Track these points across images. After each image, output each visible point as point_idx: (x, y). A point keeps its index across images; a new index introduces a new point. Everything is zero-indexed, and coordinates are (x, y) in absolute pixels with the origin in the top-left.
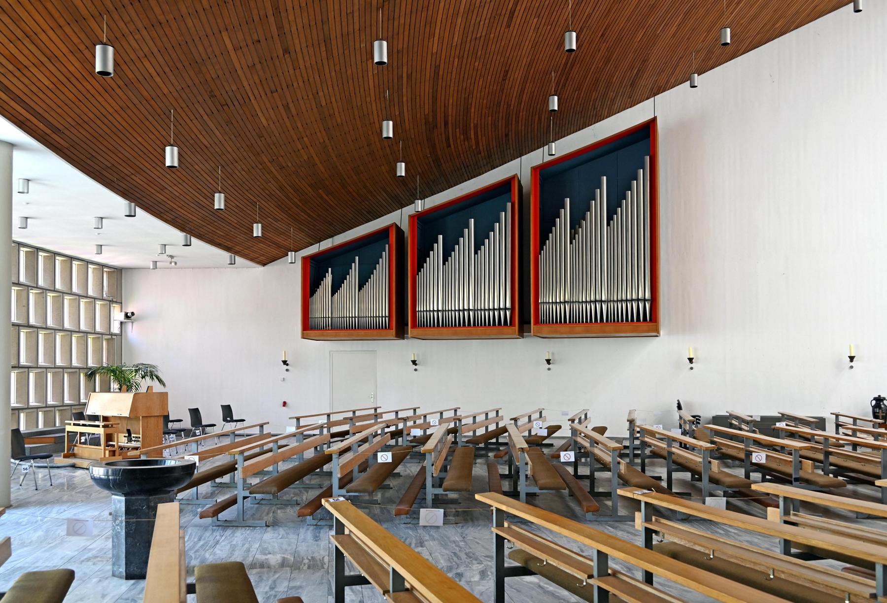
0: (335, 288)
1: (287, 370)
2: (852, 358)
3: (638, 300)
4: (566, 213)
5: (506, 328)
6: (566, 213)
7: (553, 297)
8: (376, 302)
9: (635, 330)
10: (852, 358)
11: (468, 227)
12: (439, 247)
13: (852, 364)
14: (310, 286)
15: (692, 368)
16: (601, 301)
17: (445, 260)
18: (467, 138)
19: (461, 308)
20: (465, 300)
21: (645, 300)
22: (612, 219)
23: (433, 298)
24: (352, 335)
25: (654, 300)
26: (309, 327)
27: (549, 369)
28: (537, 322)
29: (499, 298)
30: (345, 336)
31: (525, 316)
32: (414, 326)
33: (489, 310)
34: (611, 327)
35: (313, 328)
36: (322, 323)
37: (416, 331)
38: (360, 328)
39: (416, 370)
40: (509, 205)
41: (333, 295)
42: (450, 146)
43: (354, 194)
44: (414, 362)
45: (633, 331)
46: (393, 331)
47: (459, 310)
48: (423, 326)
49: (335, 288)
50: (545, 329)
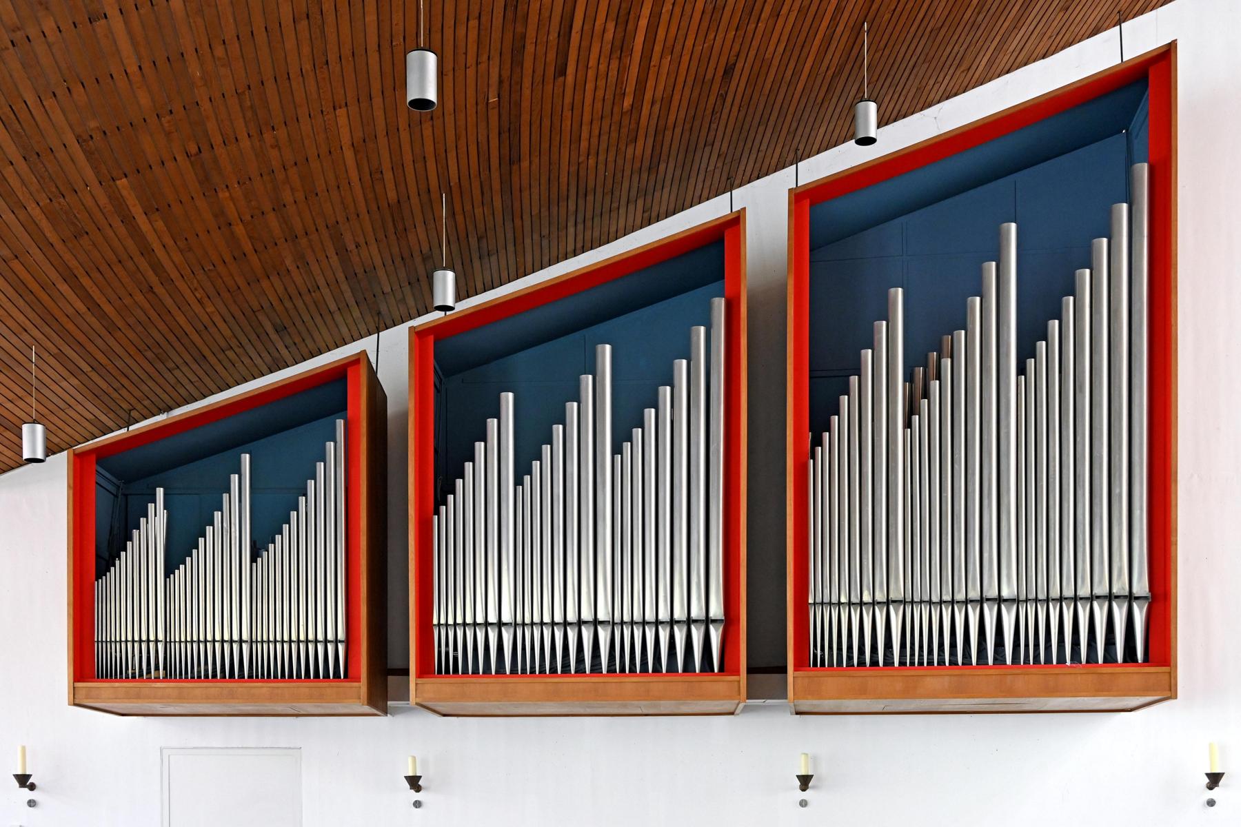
0: (178, 552)
1: (32, 803)
2: (1214, 779)
3: (1110, 597)
4: (892, 334)
5: (707, 678)
6: (892, 334)
7: (851, 588)
8: (308, 599)
9: (1101, 689)
10: (1214, 779)
11: (593, 369)
12: (503, 430)
13: (1214, 794)
14: (97, 549)
15: (1211, 803)
16: (1000, 600)
17: (522, 470)
18: (621, 47)
19: (572, 617)
20: (586, 595)
21: (1131, 598)
22: (1033, 355)
23: (482, 592)
24: (232, 696)
25: (1161, 599)
26: (91, 665)
27: (803, 803)
28: (801, 664)
29: (687, 591)
30: (208, 698)
31: (767, 645)
32: (425, 670)
33: (657, 623)
34: (1035, 676)
35: (110, 673)
36: (134, 657)
37: (434, 687)
38: (258, 673)
39: (417, 804)
40: (719, 304)
41: (169, 572)
42: (562, 72)
43: (239, 230)
44: (414, 782)
45: (1098, 691)
46: (363, 686)
47: (580, 623)
48: (450, 669)
49: (178, 552)
50: (830, 680)
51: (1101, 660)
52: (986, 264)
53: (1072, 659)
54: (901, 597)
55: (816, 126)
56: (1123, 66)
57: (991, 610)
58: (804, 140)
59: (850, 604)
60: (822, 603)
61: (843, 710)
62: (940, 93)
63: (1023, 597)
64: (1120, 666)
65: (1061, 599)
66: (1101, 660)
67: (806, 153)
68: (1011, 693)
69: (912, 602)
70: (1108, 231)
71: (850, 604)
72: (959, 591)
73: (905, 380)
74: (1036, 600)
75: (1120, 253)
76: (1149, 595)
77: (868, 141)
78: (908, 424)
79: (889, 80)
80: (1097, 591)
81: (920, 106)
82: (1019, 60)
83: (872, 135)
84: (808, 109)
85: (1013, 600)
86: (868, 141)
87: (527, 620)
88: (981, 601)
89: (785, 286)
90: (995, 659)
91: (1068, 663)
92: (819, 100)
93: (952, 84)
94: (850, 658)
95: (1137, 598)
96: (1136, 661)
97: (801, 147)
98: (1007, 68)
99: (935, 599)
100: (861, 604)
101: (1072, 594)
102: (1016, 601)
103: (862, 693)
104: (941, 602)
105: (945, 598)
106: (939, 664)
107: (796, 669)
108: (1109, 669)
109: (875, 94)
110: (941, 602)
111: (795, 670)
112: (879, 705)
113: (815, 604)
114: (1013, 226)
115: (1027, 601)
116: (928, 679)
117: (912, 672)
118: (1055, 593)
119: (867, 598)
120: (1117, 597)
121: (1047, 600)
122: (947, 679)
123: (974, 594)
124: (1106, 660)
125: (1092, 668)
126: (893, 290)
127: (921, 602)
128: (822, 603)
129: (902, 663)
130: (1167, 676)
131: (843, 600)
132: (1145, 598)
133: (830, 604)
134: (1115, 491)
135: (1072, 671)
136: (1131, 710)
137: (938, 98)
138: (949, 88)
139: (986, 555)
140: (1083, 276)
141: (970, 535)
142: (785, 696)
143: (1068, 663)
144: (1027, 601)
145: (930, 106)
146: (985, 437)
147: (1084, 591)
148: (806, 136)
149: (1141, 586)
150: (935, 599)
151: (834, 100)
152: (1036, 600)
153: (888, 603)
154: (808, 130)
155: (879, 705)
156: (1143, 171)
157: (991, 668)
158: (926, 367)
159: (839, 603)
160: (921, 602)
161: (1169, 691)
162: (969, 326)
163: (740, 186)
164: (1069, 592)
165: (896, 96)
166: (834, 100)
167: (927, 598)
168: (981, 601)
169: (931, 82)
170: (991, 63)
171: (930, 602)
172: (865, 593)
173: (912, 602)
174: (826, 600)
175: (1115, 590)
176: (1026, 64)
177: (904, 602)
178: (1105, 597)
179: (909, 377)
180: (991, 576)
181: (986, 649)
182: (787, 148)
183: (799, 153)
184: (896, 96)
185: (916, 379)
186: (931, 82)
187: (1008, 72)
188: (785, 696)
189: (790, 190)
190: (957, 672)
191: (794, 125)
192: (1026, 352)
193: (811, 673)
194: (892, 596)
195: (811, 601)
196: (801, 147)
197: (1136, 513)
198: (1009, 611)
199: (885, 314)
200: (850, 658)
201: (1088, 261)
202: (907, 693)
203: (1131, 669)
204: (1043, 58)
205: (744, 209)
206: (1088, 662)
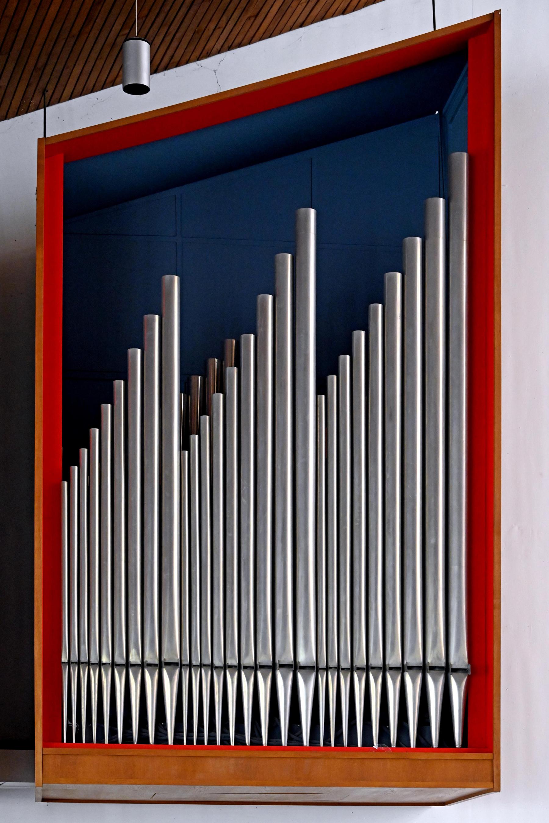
4: (166, 333)
6: (166, 333)
21: (447, 670)
28: (53, 737)
50: (90, 761)
51: (413, 744)
52: (280, 256)
53: (380, 742)
54: (177, 659)
55: (70, 64)
56: (434, 37)
57: (285, 679)
58: (54, 81)
59: (113, 664)
60: (79, 663)
61: (102, 798)
62: (221, 41)
63: (322, 664)
64: (435, 750)
65: (367, 669)
66: (413, 744)
67: (56, 96)
68: (309, 781)
69: (190, 666)
70: (422, 230)
71: (113, 664)
72: (247, 653)
73: (181, 391)
74: (338, 668)
75: (434, 259)
76: (469, 667)
77: (139, 89)
78: (185, 445)
79: (162, 16)
80: (409, 661)
81: (197, 53)
82: (262, 30)
83: (145, 82)
84: (61, 43)
85: (311, 668)
86: (139, 89)
87: (361, 661)
88: (273, 667)
89: (33, 259)
90: (290, 739)
91: (376, 746)
92: (75, 31)
93: (235, 32)
94: (338, 735)
95: (455, 671)
96: (453, 744)
97: (51, 88)
98: (301, 20)
99: (218, 662)
100: (128, 665)
101: (380, 663)
102: (314, 668)
103: (129, 776)
104: (225, 667)
105: (230, 662)
106: (222, 742)
107: (45, 745)
108: (423, 755)
109: (144, 32)
110: (225, 667)
111: (45, 745)
112: (148, 792)
113: (69, 663)
114: (312, 212)
115: (327, 668)
116: (210, 761)
117: (191, 753)
118: (361, 661)
119: (134, 658)
120: (432, 668)
121: (351, 669)
122: (232, 761)
123: (265, 659)
124: (419, 744)
125: (403, 753)
126: (167, 277)
127: (201, 666)
128: (79, 663)
129: (178, 740)
130: (488, 765)
131: (104, 660)
132: (464, 670)
133: (89, 663)
134: (430, 541)
135: (380, 755)
136: (444, 804)
137: (218, 46)
138: (232, 37)
139: (279, 611)
140: (265, 302)
141: (260, 586)
142: (32, 779)
143: (376, 746)
144: (327, 668)
145: (209, 55)
146: (278, 467)
147: (394, 660)
148: (56, 74)
149: (460, 657)
150: (218, 662)
151: (95, 32)
152: (338, 668)
153: (160, 665)
154: (59, 67)
155: (148, 792)
156: (462, 161)
157: (284, 749)
158: (205, 376)
159: (100, 664)
160: (201, 666)
161: (490, 782)
162: (260, 331)
163: (81, 95)
164: (376, 660)
165: (168, 38)
166: (95, 32)
167: (207, 661)
168: (273, 667)
169: (212, 26)
170: (282, 12)
171: (212, 666)
172: (133, 652)
173: (190, 666)
174: (84, 659)
175: (429, 660)
176: (322, 19)
177: (180, 665)
178: (418, 668)
179: (186, 387)
180: (285, 637)
181: (355, 724)
182: (32, 88)
183: (48, 95)
184: (168, 38)
185: (193, 391)
186: (212, 26)
187: (301, 26)
188: (32, 779)
189: (39, 140)
190: (245, 753)
191: (43, 59)
192: (327, 367)
193: (64, 751)
194: (166, 657)
195: (64, 659)
196: (51, 88)
197: (454, 569)
198: (306, 681)
199: (158, 306)
200: (338, 735)
201: (399, 264)
202: (184, 778)
203: (448, 755)
204: (344, 13)
205: (500, 11)
206: (398, 745)
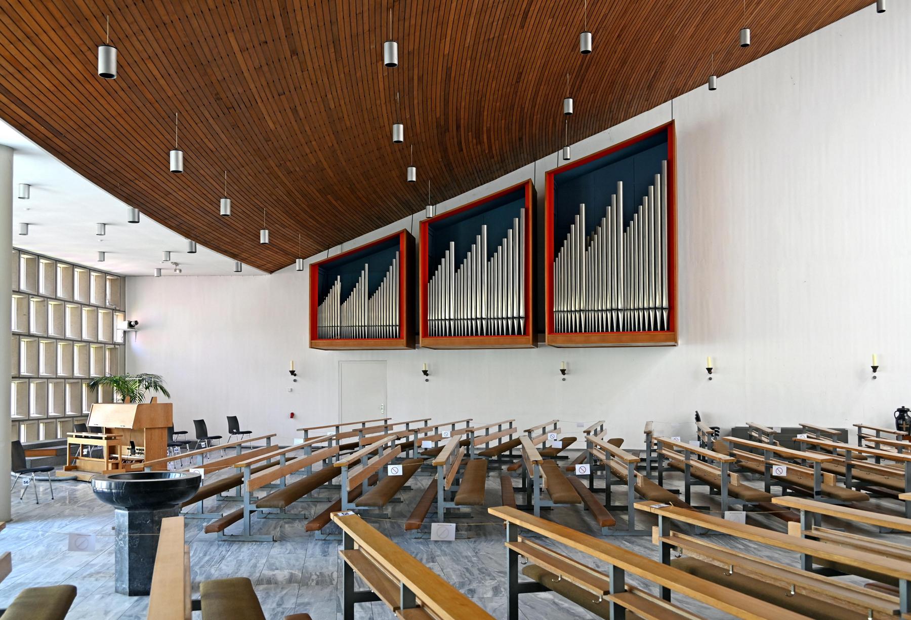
0: (344, 296)
1: (295, 381)
2: (875, 369)
3: (655, 308)
4: (581, 219)
5: (519, 337)
6: (581, 219)
7: (568, 305)
8: (386, 310)
9: (652, 340)
10: (875, 369)
11: (480, 233)
12: (451, 254)
13: (875, 374)
14: (319, 295)
15: (710, 379)
16: (618, 310)
17: (457, 268)
18: (480, 142)
19: (474, 317)
20: (477, 308)
21: (662, 309)
22: (629, 226)
23: (445, 306)
24: (362, 345)
25: (672, 308)
26: (317, 336)
27: (564, 380)
28: (551, 331)
29: (512, 307)
30: (354, 345)
31: (539, 325)
32: (425, 335)
33: (502, 318)
34: (627, 336)
35: (322, 338)
36: (330, 332)
37: (428, 341)
38: (369, 337)
39: (427, 380)
40: (523, 211)
41: (342, 303)
42: (462, 150)
43: (364, 199)
44: (425, 373)
45: (650, 341)
46: (404, 341)
47: (472, 319)
48: (434, 335)
49: (344, 296)
50: (560, 338)
